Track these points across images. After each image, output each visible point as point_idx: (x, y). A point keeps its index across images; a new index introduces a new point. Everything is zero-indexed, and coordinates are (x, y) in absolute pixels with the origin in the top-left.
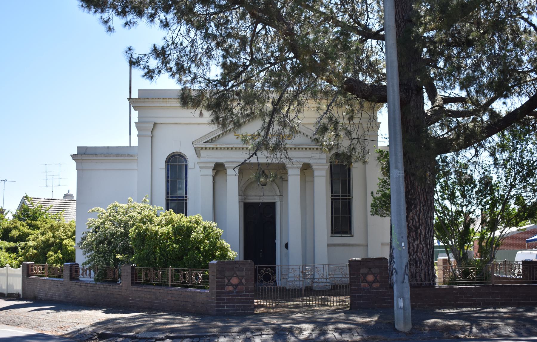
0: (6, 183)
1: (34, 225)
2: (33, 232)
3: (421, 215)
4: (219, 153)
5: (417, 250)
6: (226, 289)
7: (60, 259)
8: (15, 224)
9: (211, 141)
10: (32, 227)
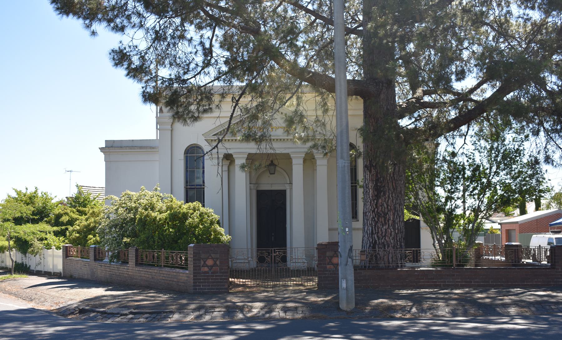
0: (72, 173)
1: (83, 211)
2: (80, 217)
3: (389, 201)
5: (385, 235)
6: (202, 270)
7: (98, 241)
8: (66, 211)
10: (81, 213)
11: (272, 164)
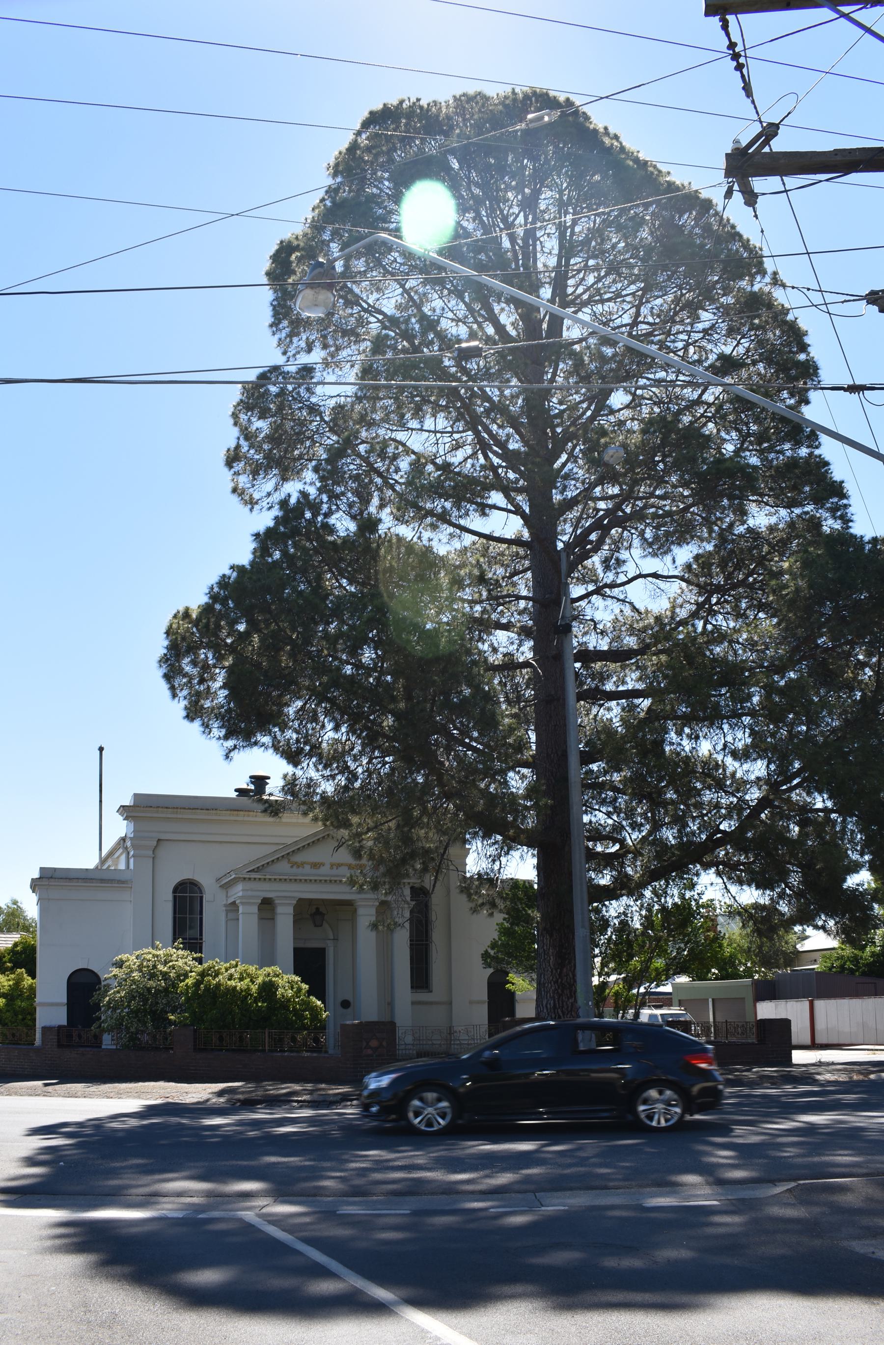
4: (266, 886)
9: (257, 870)
11: (318, 912)
